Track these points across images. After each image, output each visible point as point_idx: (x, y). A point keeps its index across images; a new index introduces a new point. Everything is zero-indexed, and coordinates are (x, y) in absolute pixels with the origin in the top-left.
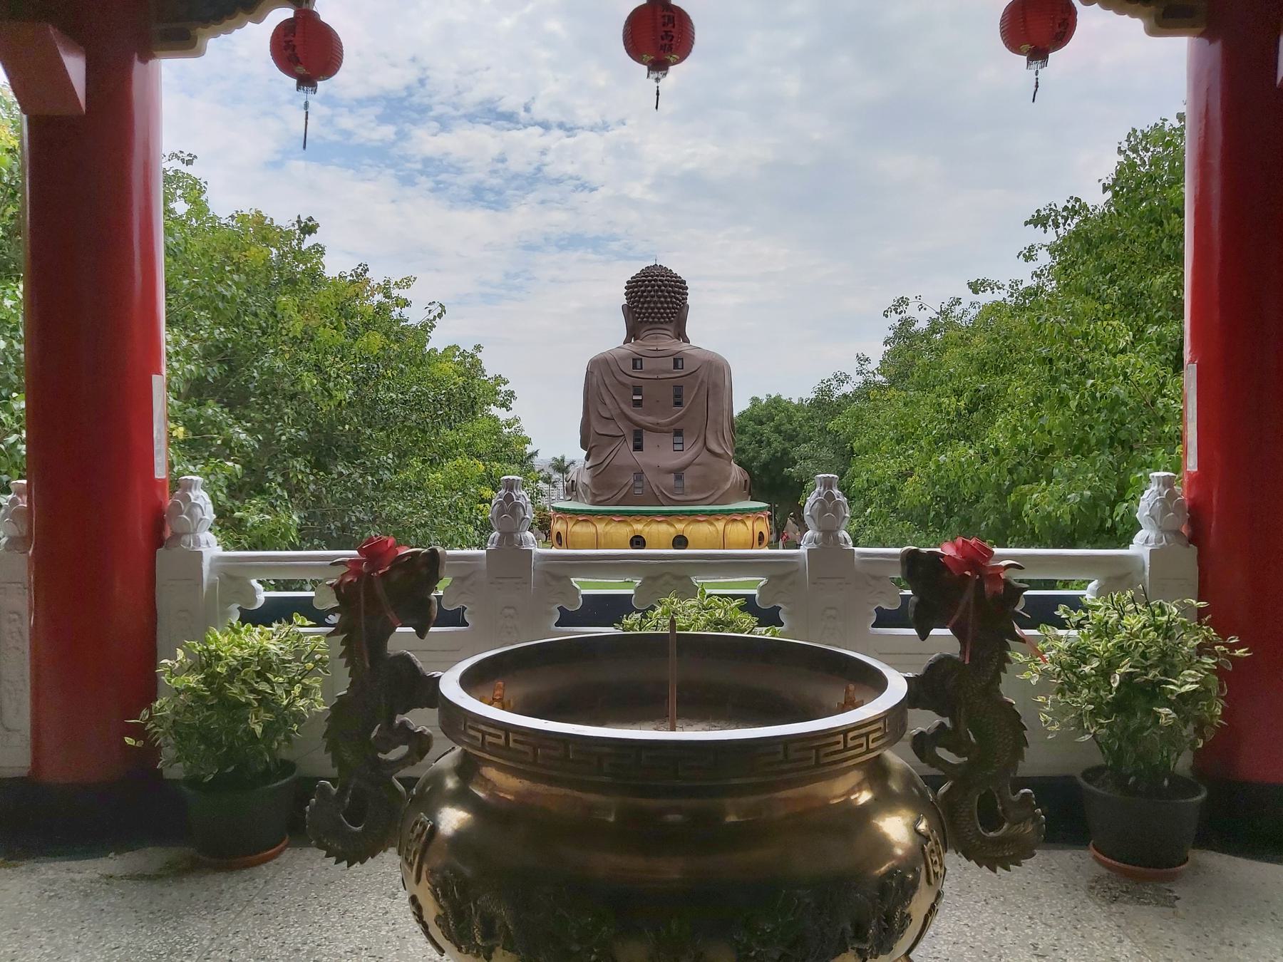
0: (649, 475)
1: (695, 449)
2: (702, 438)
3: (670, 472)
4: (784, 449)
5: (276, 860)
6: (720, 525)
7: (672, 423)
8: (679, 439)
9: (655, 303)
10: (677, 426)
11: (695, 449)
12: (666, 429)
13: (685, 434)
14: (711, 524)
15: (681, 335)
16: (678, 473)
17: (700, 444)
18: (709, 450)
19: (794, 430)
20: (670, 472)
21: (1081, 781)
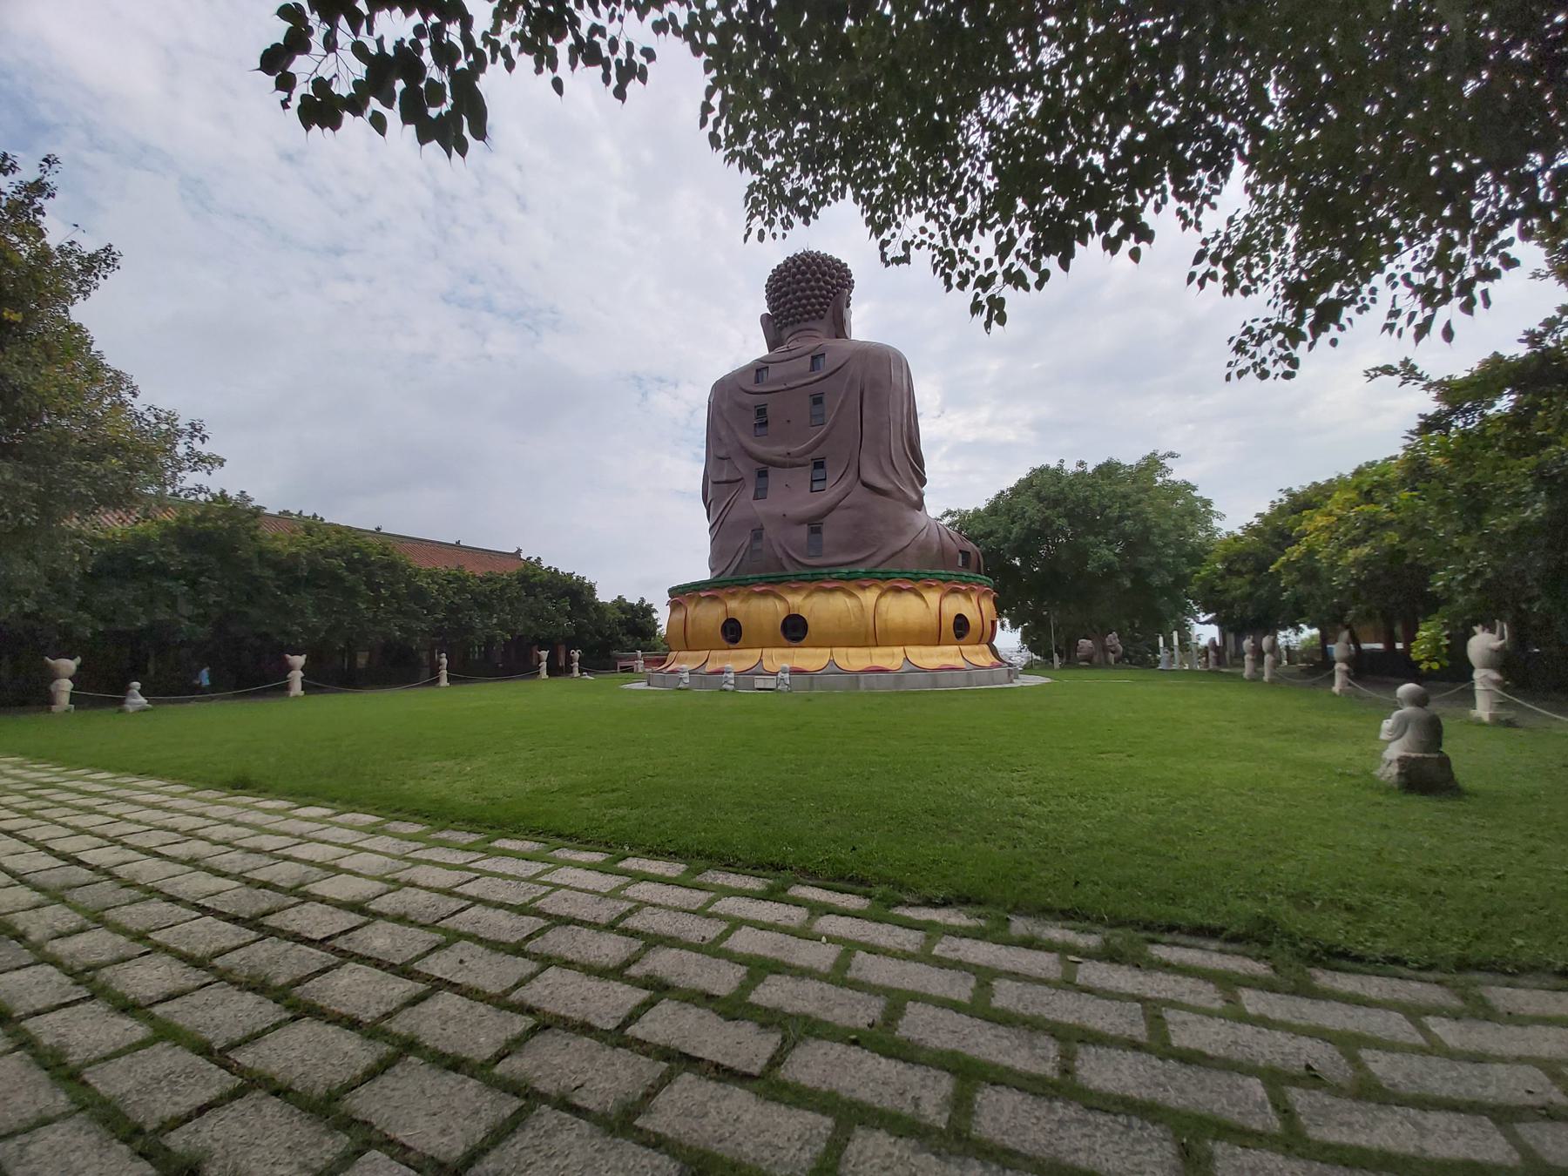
0: (770, 532)
1: (843, 485)
2: (854, 468)
3: (801, 522)
4: (1046, 519)
5: (1179, 978)
6: (869, 597)
7: (808, 451)
8: (819, 474)
9: (808, 298)
10: (816, 454)
11: (843, 485)
12: (799, 461)
13: (827, 463)
14: (850, 594)
15: (839, 327)
16: (814, 524)
17: (851, 476)
18: (865, 484)
19: (1062, 491)
20: (801, 522)
21: (397, 105)
